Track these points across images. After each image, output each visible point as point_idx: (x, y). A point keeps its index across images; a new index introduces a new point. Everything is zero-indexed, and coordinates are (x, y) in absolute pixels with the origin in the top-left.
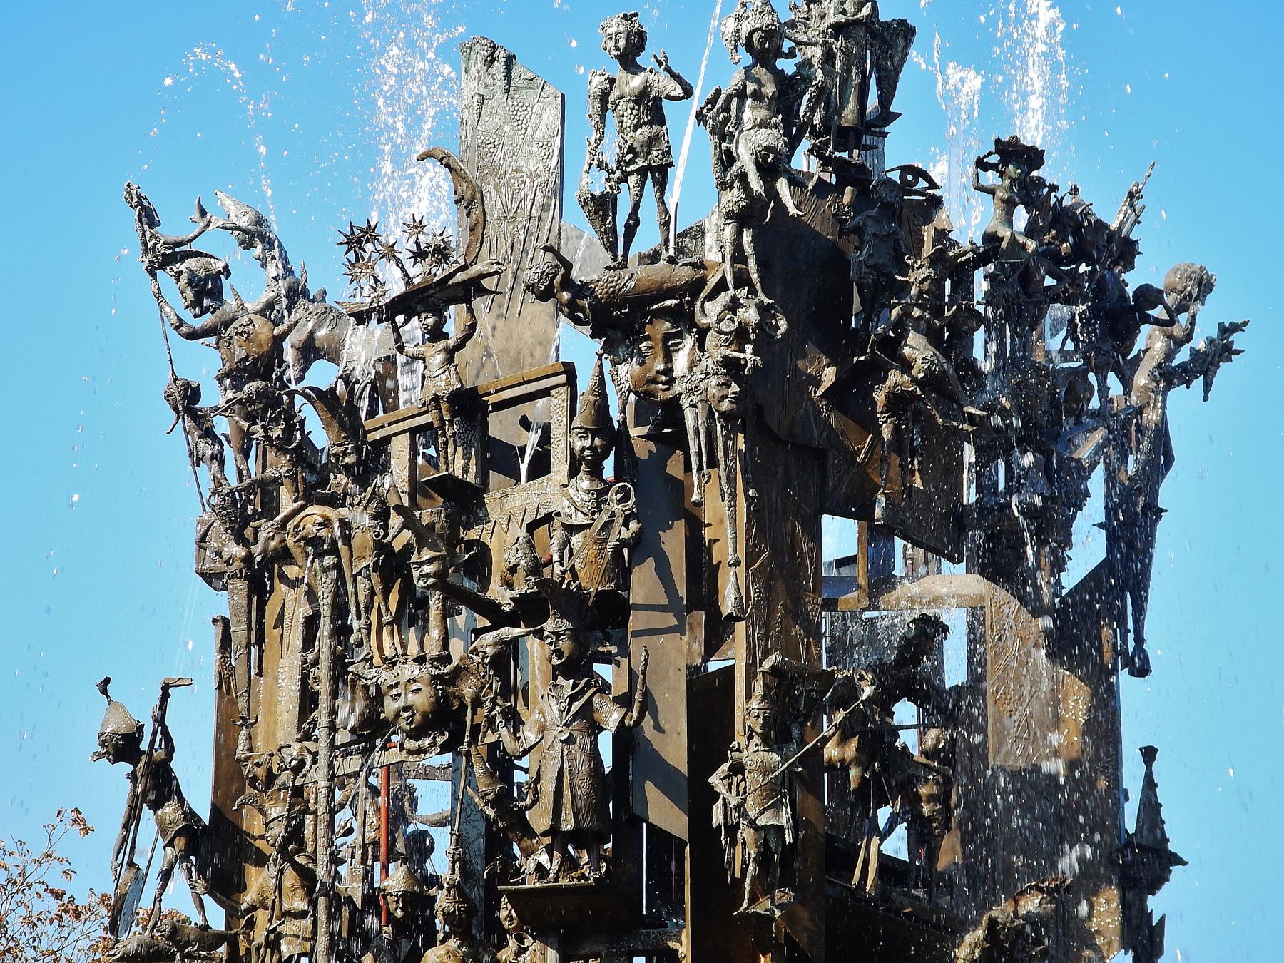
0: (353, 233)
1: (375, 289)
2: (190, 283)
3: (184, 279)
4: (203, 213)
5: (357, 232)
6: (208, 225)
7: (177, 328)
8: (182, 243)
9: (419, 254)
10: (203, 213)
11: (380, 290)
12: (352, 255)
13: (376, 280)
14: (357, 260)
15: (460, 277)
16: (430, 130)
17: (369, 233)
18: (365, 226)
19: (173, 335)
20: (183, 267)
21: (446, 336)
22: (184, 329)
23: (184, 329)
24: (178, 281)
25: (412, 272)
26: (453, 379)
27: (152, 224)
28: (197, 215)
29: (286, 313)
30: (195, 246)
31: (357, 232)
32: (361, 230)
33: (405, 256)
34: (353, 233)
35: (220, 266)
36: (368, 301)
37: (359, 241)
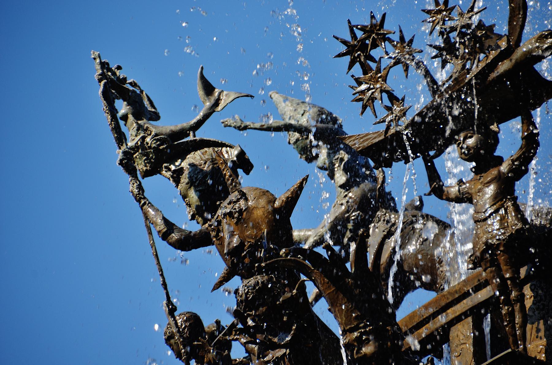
0: (354, 36)
1: (389, 109)
2: (191, 183)
3: (185, 179)
4: (208, 89)
5: (360, 34)
6: (217, 103)
7: (165, 236)
8: (183, 133)
9: (447, 50)
10: (208, 89)
11: (397, 109)
12: (357, 70)
13: (392, 98)
14: (365, 73)
15: (504, 66)
16: (534, 187)
17: (375, 33)
18: (367, 22)
19: (162, 246)
20: (185, 164)
21: (500, 160)
22: (175, 236)
23: (175, 236)
24: (177, 181)
25: (441, 76)
26: (511, 217)
27: (142, 111)
28: (201, 92)
29: (397, 249)
30: (201, 134)
31: (360, 34)
32: (363, 29)
33: (502, 202)
34: (354, 36)
35: (231, 154)
36: (382, 127)
37: (363, 47)
